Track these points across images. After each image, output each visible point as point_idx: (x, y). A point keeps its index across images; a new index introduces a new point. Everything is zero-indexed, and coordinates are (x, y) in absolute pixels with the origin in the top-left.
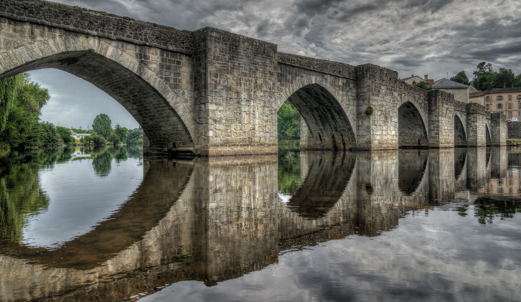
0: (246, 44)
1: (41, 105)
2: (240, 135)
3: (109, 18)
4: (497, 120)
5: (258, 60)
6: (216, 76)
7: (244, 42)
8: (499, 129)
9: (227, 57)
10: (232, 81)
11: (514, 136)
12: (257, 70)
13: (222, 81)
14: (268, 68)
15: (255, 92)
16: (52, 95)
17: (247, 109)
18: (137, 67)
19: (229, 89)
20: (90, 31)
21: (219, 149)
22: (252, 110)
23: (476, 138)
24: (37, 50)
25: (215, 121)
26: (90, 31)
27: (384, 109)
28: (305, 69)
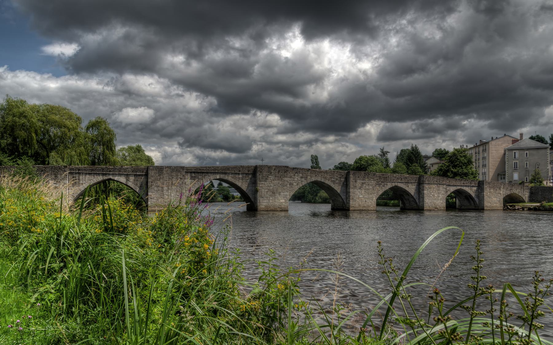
0: (167, 169)
1: (447, 152)
2: (163, 203)
3: (114, 172)
4: (482, 186)
5: (174, 174)
6: (152, 182)
7: (166, 168)
8: (484, 195)
9: (157, 175)
10: (159, 183)
11: (534, 200)
12: (173, 178)
13: (154, 184)
14: (179, 177)
15: (171, 187)
16: (140, 144)
17: (167, 193)
18: (125, 181)
19: (158, 186)
20: (110, 173)
21: (153, 208)
22: (169, 194)
23: (424, 203)
24: (95, 180)
25: (151, 198)
26: (110, 173)
27: (271, 188)
28: (211, 173)
